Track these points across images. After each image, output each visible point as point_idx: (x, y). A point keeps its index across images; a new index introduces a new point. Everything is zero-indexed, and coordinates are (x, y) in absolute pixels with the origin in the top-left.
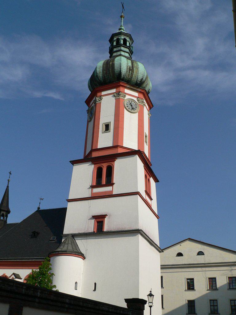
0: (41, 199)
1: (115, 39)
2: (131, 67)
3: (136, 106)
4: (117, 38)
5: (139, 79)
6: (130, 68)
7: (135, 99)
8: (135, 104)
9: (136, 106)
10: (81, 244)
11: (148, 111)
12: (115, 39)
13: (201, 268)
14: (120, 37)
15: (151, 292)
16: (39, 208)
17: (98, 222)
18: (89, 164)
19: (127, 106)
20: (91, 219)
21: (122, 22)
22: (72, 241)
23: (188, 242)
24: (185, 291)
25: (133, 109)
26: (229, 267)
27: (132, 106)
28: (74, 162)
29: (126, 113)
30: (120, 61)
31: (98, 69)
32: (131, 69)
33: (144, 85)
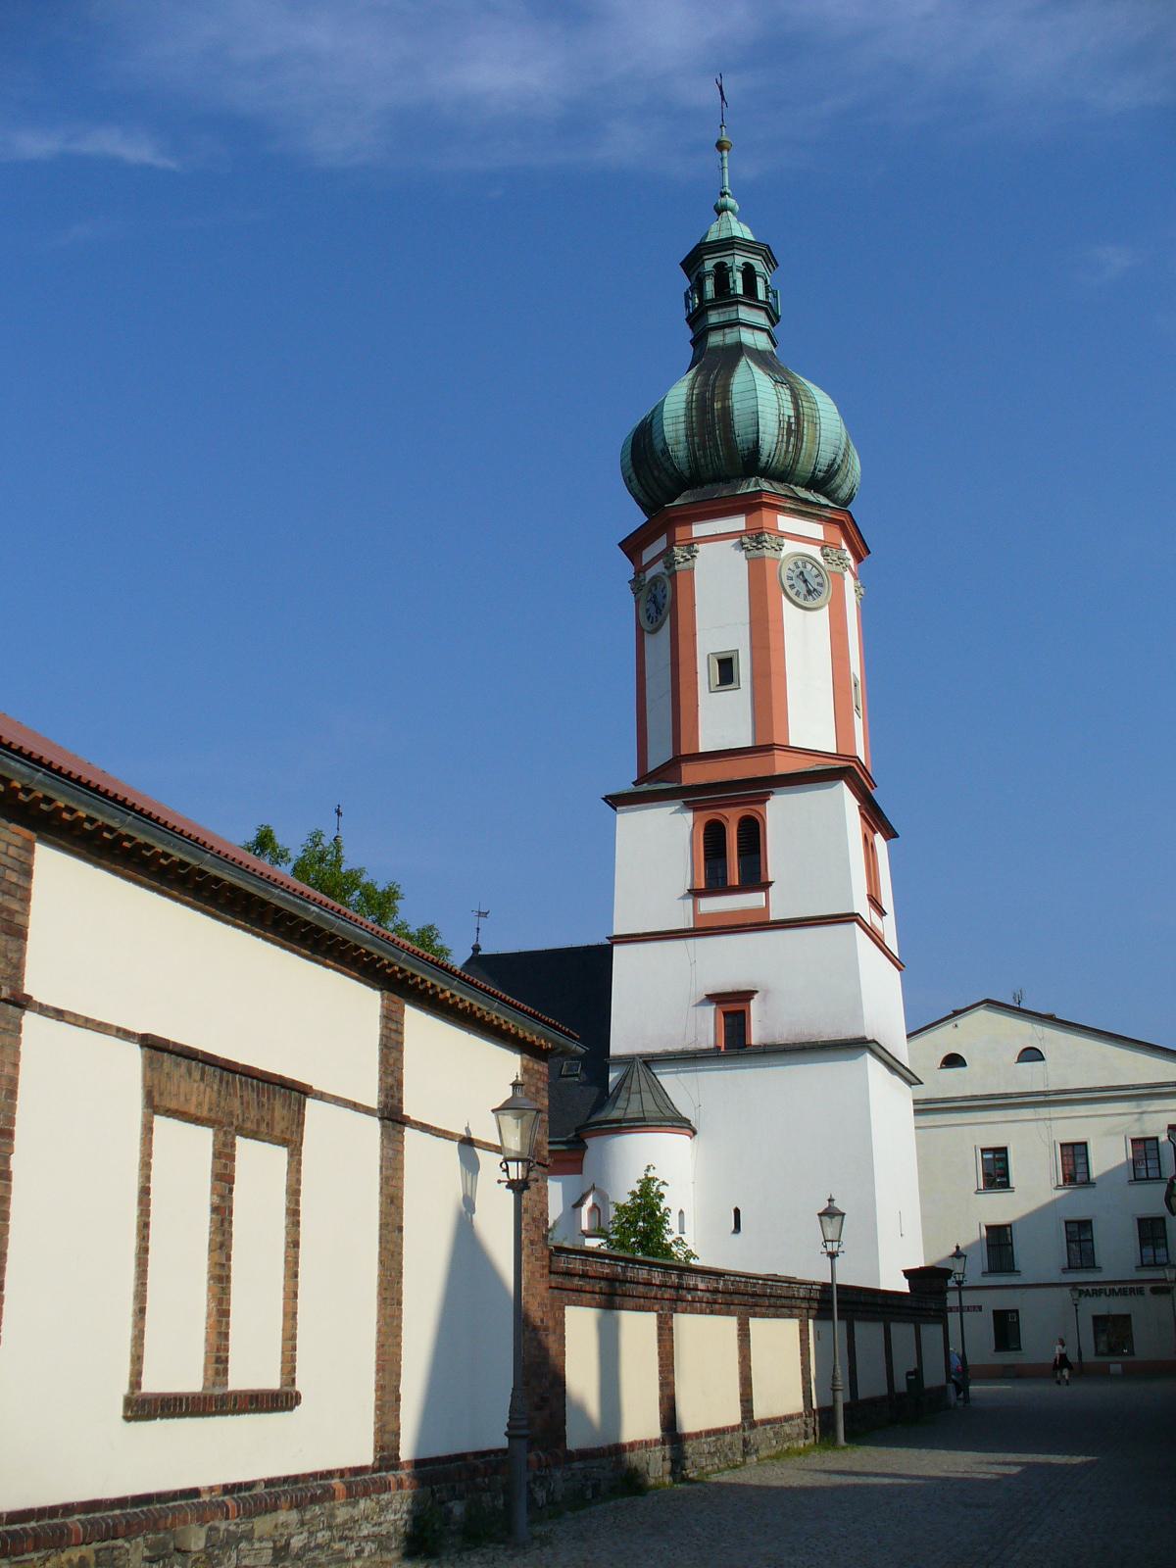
0: (483, 914)
1: (709, 265)
2: (793, 420)
3: (819, 580)
4: (718, 260)
5: (824, 461)
6: (789, 424)
7: (815, 552)
8: (815, 572)
9: (819, 580)
10: (677, 1085)
11: (856, 579)
12: (709, 265)
13: (1032, 1110)
14: (727, 260)
15: (831, 1200)
16: (476, 949)
17: (726, 1014)
18: (673, 809)
19: (792, 586)
20: (702, 1003)
21: (726, 170)
22: (650, 1083)
23: (982, 1014)
24: (976, 1193)
25: (809, 592)
26: (1133, 1104)
27: (805, 581)
28: (616, 801)
29: (789, 611)
30: (753, 402)
31: (671, 428)
32: (794, 430)
33: (838, 480)
